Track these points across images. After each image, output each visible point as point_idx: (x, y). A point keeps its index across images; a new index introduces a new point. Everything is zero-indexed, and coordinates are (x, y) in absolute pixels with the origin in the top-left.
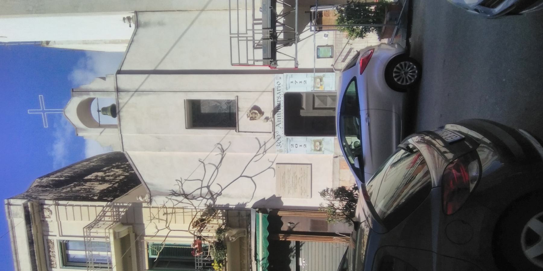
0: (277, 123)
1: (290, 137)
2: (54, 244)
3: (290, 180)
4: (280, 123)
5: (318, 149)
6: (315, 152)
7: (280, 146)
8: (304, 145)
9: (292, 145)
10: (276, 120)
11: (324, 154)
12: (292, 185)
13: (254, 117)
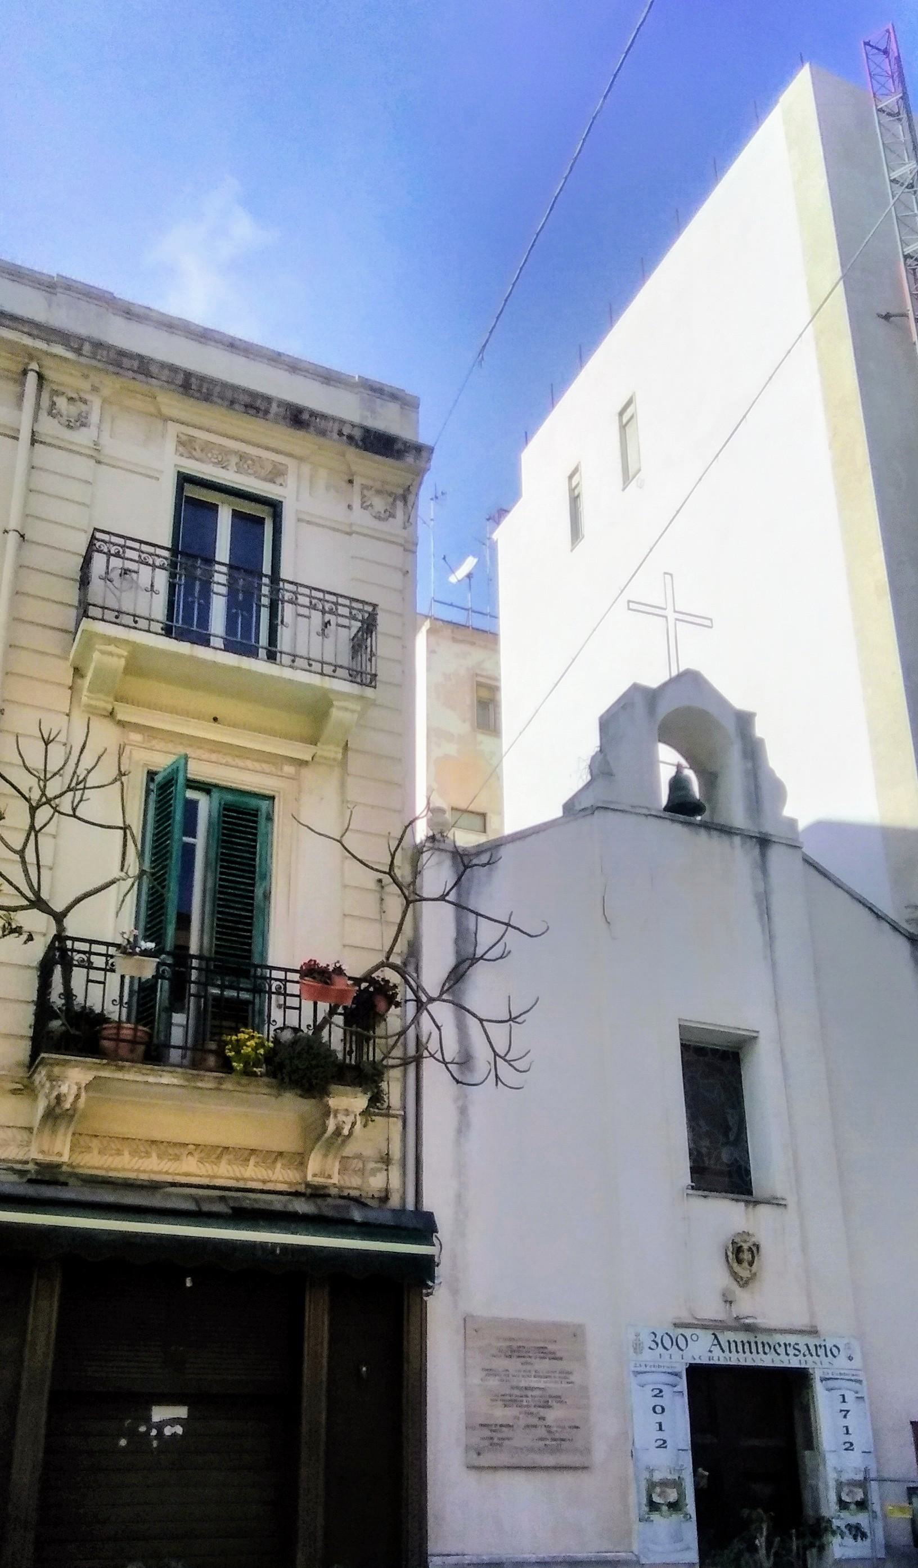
0: (724, 1337)
1: (683, 1385)
2: (265, 479)
3: (533, 1379)
4: (723, 1351)
5: (656, 1499)
6: (644, 1485)
7: (654, 1346)
8: (665, 1442)
9: (661, 1391)
10: (731, 1336)
11: (640, 1520)
12: (517, 1388)
13: (741, 1255)
